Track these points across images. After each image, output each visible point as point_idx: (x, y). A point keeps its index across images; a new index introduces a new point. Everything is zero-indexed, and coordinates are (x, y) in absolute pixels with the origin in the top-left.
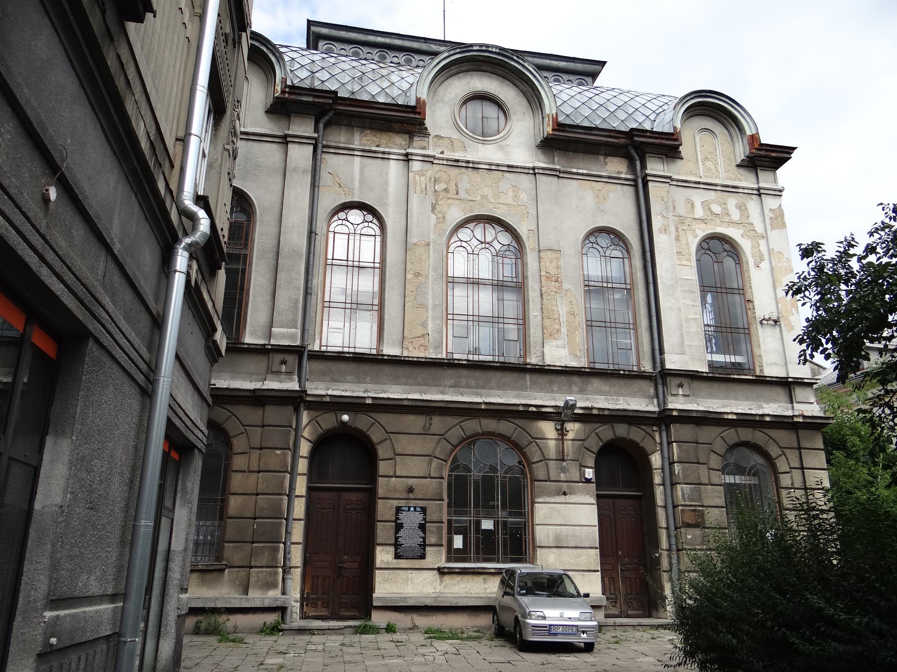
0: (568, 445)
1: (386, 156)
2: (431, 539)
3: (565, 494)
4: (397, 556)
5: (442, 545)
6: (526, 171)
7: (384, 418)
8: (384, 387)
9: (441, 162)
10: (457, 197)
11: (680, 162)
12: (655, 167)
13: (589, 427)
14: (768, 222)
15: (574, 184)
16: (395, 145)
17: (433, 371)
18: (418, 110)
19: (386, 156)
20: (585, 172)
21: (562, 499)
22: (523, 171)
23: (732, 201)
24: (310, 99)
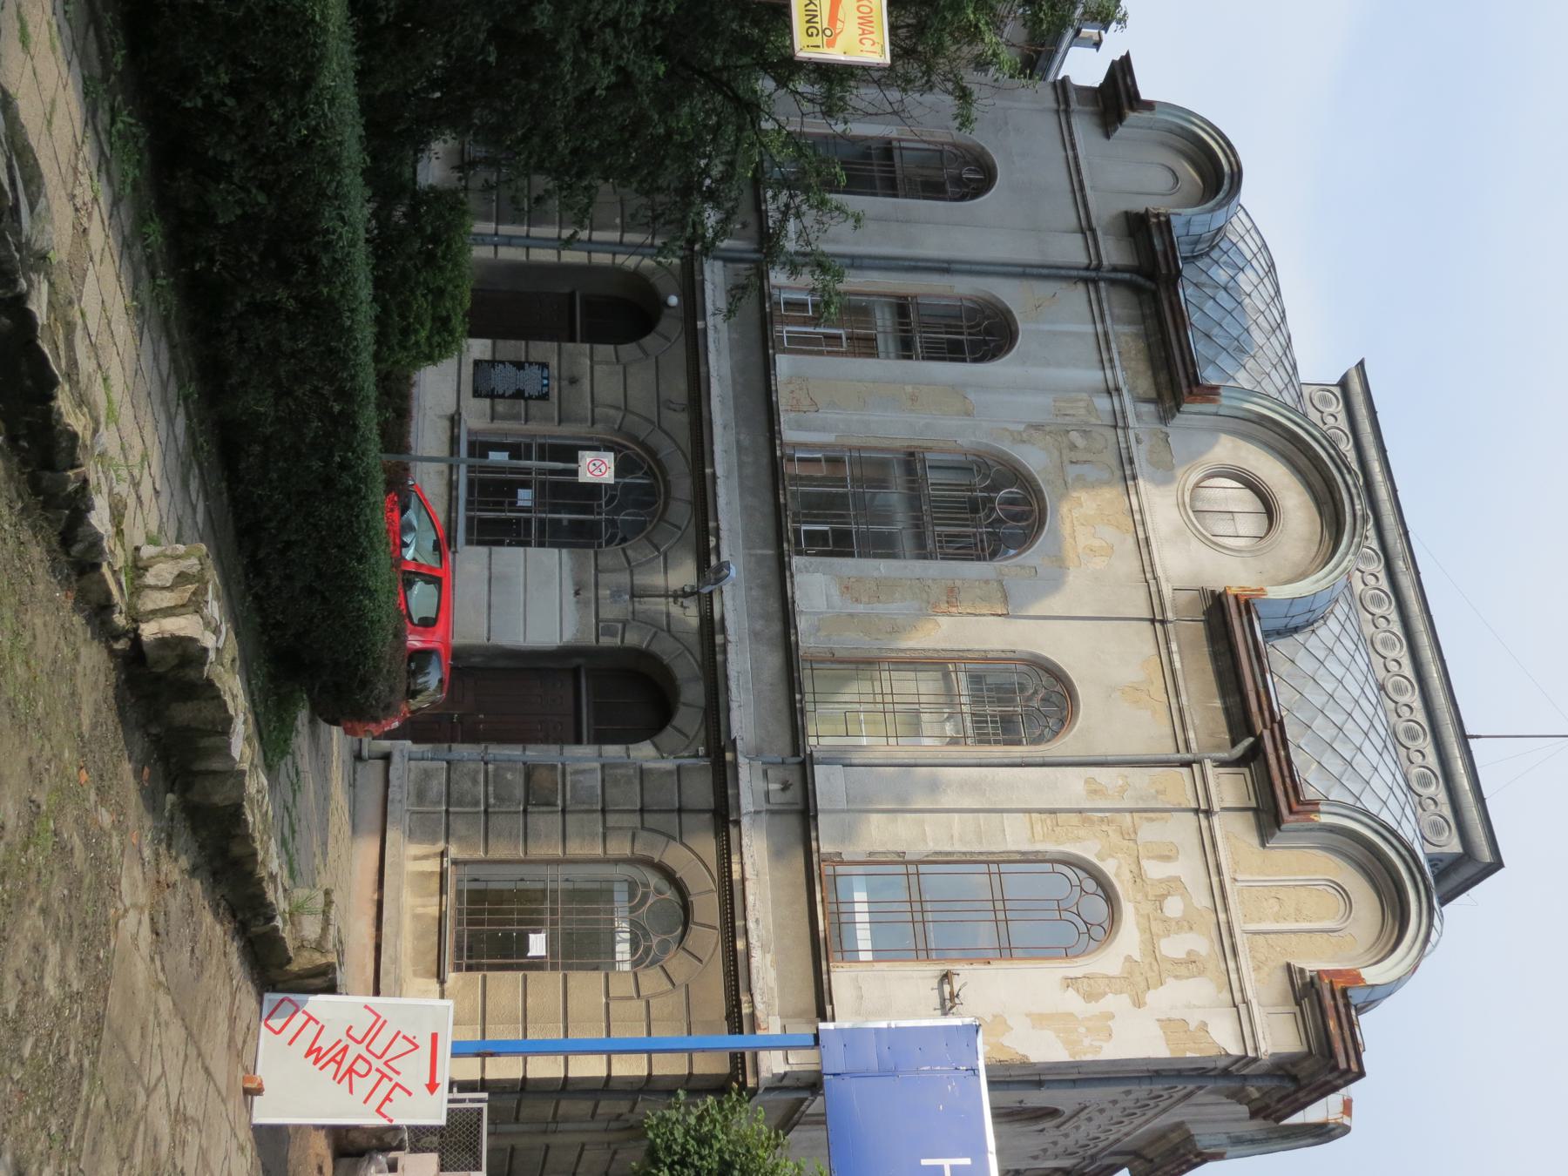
1: (1107, 365)
2: (501, 406)
3: (577, 593)
4: (477, 363)
5: (493, 419)
6: (1148, 569)
7: (680, 350)
8: (726, 352)
9: (1121, 439)
10: (1066, 462)
11: (1254, 840)
12: (1228, 788)
13: (693, 640)
15: (1150, 649)
16: (1132, 373)
17: (762, 418)
18: (1195, 390)
19: (1107, 365)
20: (1178, 665)
21: (569, 589)
22: (1146, 563)
23: (1201, 943)
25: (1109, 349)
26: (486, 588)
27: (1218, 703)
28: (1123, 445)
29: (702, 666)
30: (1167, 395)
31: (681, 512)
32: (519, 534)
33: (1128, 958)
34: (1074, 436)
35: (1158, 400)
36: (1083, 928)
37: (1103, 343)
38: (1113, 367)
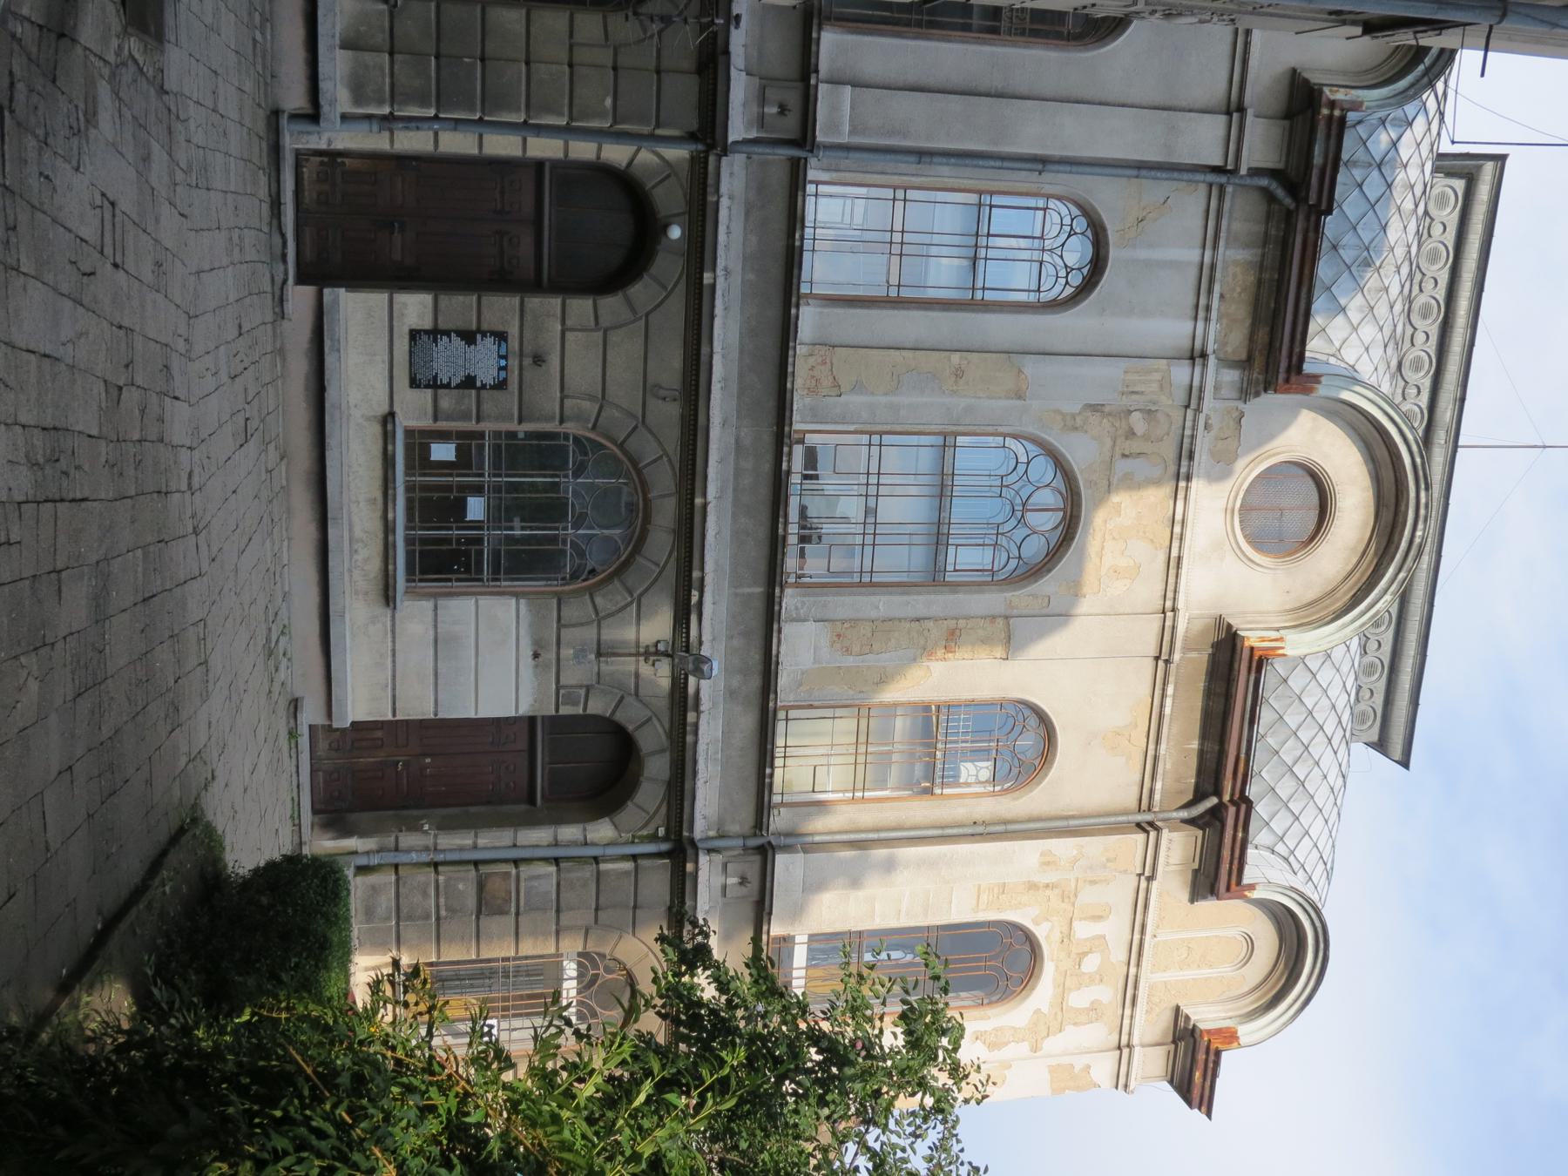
0: (628, 665)
1: (1201, 314)
2: (447, 401)
3: (536, 656)
4: (414, 335)
5: (436, 419)
6: (1170, 595)
7: (676, 307)
9: (1189, 424)
12: (1178, 848)
13: (662, 704)
14: (1066, 1060)
16: (1226, 330)
17: (771, 404)
18: (1293, 378)
19: (1201, 314)
20: (1168, 710)
21: (527, 652)
22: (1171, 587)
23: (1108, 994)
24: (1318, 159)
25: (1210, 291)
26: (432, 652)
27: (1195, 745)
28: (1188, 432)
29: (670, 736)
30: (1259, 362)
31: (661, 542)
32: (468, 571)
33: (1038, 1011)
34: (1136, 417)
35: (1246, 364)
36: (1063, 273)
37: (1206, 277)
38: (1207, 319)
